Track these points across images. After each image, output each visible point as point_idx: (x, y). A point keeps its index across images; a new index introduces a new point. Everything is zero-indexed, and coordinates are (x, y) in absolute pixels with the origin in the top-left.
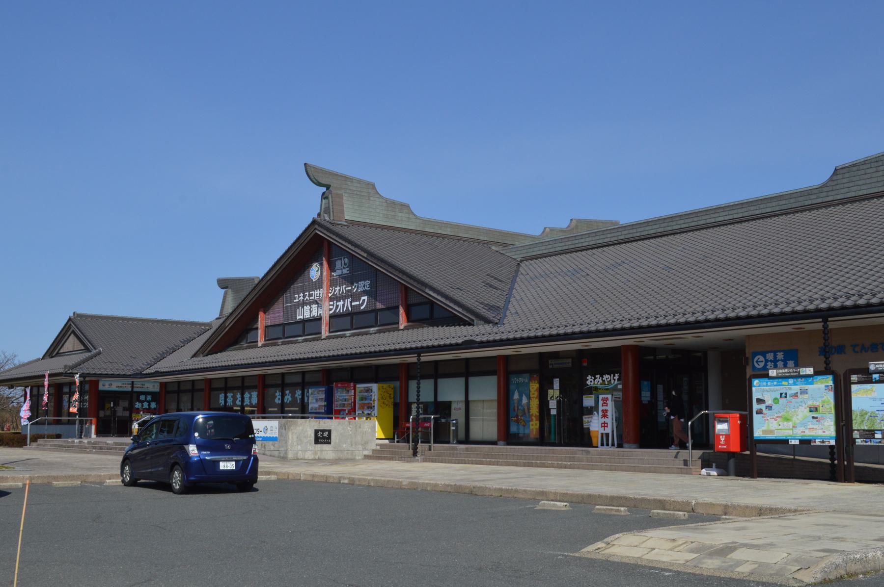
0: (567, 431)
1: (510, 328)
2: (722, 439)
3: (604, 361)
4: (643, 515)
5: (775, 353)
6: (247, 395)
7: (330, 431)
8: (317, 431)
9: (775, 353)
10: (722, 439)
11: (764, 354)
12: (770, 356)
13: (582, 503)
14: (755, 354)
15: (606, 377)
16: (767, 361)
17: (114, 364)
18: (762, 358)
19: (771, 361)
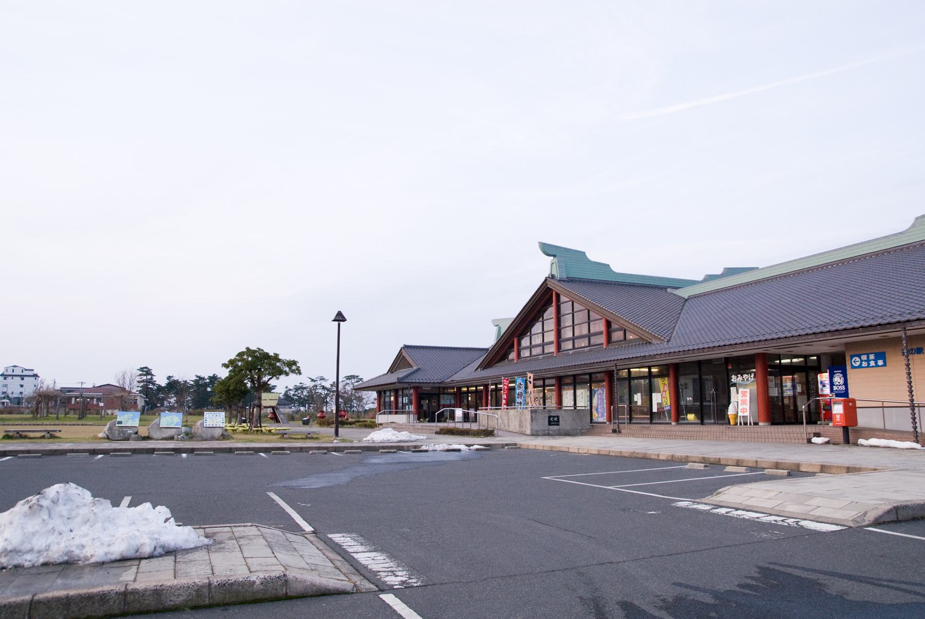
0: (712, 410)
1: (676, 345)
2: (838, 417)
3: (742, 364)
4: (756, 473)
5: (868, 355)
6: (568, 396)
7: (558, 417)
8: (550, 417)
9: (868, 355)
10: (838, 417)
11: (859, 356)
12: (864, 357)
13: (715, 465)
14: (852, 357)
15: (745, 376)
16: (862, 361)
17: (430, 375)
18: (858, 359)
19: (650, 372)
